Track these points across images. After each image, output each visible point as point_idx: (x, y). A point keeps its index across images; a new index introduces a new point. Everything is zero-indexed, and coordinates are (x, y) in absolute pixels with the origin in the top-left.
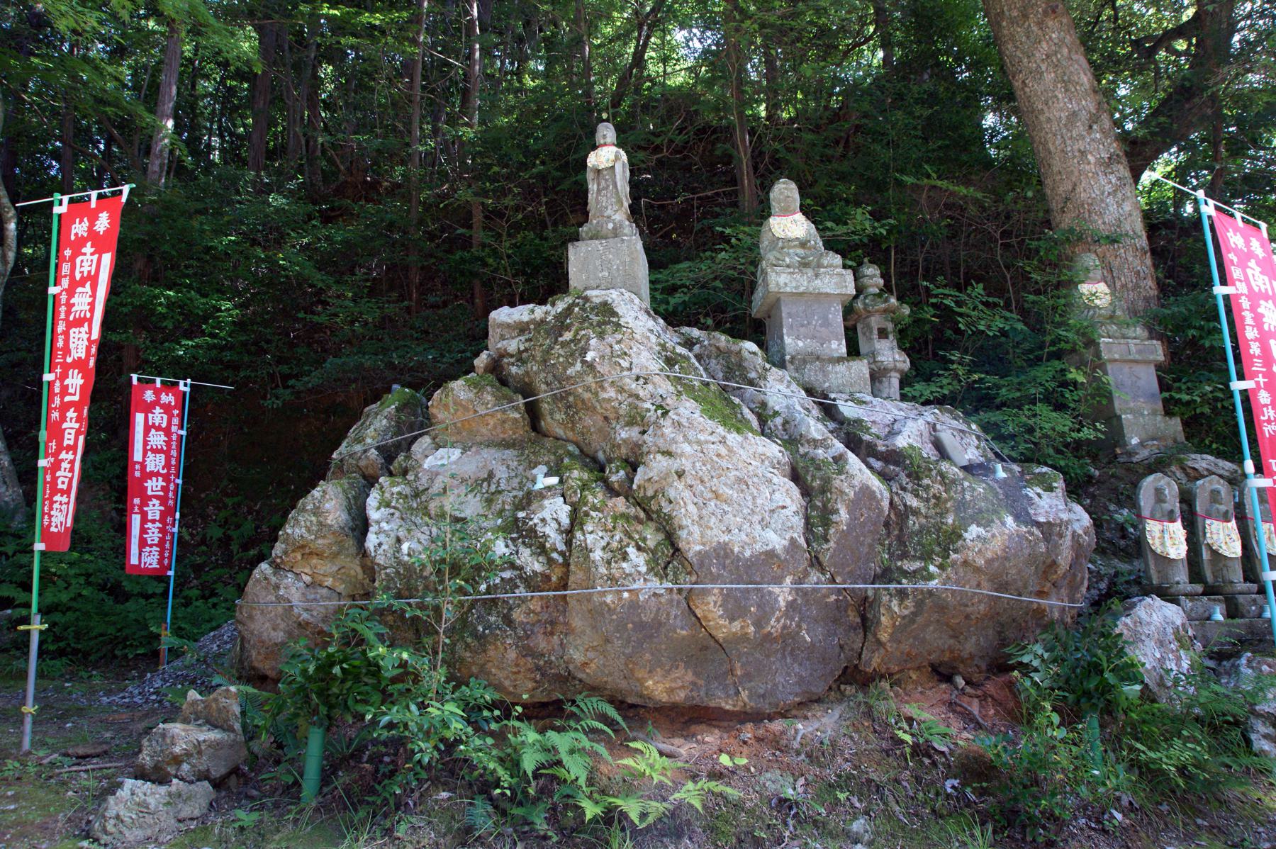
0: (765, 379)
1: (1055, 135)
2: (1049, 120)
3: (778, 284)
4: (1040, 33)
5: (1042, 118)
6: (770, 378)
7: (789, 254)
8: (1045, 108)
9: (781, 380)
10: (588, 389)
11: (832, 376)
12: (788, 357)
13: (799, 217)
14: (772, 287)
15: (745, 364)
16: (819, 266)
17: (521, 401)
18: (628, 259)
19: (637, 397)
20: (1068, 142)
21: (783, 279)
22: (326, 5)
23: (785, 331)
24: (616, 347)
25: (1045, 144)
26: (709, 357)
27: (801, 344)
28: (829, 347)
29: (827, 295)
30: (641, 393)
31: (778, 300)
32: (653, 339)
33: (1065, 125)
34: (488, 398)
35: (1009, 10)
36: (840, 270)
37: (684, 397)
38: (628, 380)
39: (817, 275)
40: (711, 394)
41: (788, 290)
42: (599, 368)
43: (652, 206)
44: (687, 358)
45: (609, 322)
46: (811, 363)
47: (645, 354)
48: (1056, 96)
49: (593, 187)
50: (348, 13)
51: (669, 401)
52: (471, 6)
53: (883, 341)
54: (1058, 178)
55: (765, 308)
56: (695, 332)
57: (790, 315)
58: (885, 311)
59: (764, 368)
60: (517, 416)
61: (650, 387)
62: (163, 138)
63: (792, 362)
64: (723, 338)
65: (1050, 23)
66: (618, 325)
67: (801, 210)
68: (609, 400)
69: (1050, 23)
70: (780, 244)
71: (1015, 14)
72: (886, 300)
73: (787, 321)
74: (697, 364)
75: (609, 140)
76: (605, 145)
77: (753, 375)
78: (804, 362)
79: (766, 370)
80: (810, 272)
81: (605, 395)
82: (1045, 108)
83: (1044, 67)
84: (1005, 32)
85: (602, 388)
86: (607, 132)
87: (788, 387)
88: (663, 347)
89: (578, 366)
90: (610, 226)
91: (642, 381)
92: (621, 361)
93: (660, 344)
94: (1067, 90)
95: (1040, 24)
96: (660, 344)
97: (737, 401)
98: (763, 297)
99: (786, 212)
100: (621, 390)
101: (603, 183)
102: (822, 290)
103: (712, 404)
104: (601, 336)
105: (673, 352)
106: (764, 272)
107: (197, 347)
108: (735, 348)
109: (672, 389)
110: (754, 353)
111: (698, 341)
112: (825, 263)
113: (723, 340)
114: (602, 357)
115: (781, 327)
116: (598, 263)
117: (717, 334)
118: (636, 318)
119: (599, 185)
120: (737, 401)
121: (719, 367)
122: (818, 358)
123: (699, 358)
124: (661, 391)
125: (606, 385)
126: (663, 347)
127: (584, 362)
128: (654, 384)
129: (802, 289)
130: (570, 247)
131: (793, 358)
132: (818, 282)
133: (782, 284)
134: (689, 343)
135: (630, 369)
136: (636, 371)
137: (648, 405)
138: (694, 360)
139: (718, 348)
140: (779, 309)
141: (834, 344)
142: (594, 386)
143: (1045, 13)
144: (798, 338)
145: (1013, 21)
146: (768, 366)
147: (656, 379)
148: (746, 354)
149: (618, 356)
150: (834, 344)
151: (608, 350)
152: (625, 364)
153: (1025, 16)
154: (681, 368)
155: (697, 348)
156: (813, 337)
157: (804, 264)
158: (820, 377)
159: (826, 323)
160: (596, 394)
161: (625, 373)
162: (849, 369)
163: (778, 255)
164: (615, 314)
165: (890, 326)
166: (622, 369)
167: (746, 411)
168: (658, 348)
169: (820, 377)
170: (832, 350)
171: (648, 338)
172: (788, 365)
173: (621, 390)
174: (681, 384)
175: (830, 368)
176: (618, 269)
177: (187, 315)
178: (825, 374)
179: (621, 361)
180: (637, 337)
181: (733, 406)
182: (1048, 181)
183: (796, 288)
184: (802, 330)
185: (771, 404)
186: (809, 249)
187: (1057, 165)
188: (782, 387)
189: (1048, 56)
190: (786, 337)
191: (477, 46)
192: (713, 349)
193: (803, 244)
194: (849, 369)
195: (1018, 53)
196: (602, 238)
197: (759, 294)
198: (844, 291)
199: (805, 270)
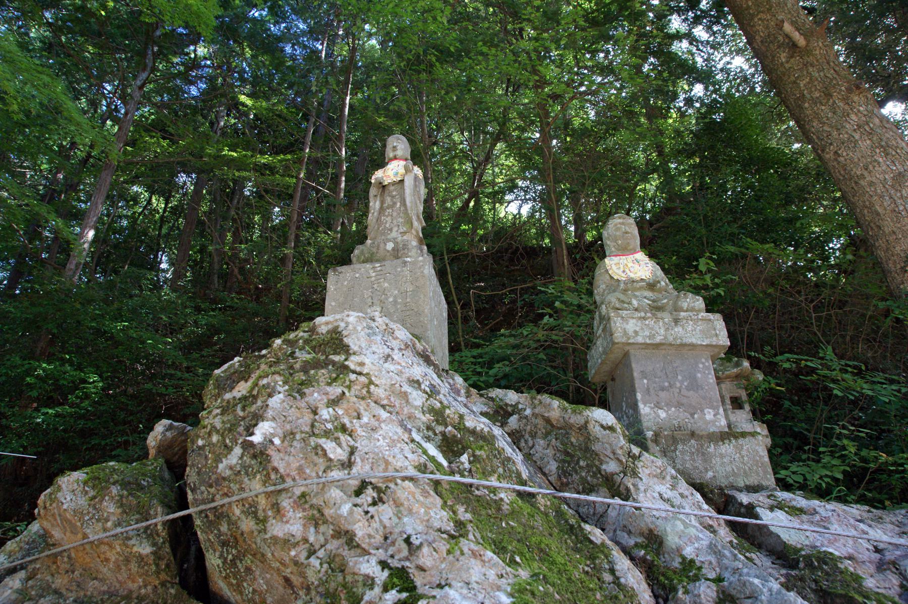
0: (635, 474)
1: (882, 197)
2: (871, 184)
3: (625, 332)
4: (846, 107)
5: (863, 183)
6: (643, 472)
7: (636, 297)
8: (866, 174)
9: (661, 477)
10: (252, 510)
11: (716, 461)
12: (649, 434)
13: (641, 256)
14: (618, 337)
15: (596, 447)
16: (677, 309)
17: (160, 518)
18: (410, 288)
19: (349, 539)
20: (899, 202)
21: (632, 326)
22: (226, 148)
23: (639, 396)
24: (325, 413)
25: (871, 207)
26: (533, 436)
27: (662, 414)
28: (702, 418)
29: (693, 346)
30: (360, 530)
31: (626, 355)
32: (417, 398)
33: (893, 186)
34: (110, 508)
35: (810, 93)
36: (704, 314)
37: (466, 545)
38: (335, 493)
39: (676, 321)
40: (538, 522)
41: (640, 339)
42: (277, 461)
43: (479, 296)
44: (488, 439)
45: (325, 364)
46: (684, 441)
47: (391, 429)
48: (876, 161)
49: (375, 205)
50: (245, 156)
51: (426, 557)
52: (341, 150)
53: (738, 412)
54: (891, 238)
55: (606, 368)
56: (511, 397)
57: (644, 375)
58: (737, 377)
59: (629, 453)
60: (146, 549)
61: (385, 512)
62: (84, 243)
63: (656, 441)
64: (556, 403)
65: (856, 98)
66: (344, 369)
67: (643, 246)
68: (287, 543)
69: (856, 98)
70: (622, 285)
71: (817, 94)
72: (737, 365)
73: (641, 384)
74: (509, 451)
75: (399, 153)
76: (395, 158)
77: (611, 467)
78: (675, 440)
79: (635, 458)
80: (667, 318)
81: (277, 529)
82: (866, 174)
83: (857, 136)
84: (809, 112)
85: (277, 508)
86: (398, 145)
87: (673, 487)
88: (439, 415)
89: (234, 457)
90: (390, 246)
91: (370, 494)
92: (329, 445)
93: (432, 410)
94: (887, 154)
95: (845, 100)
96: (432, 410)
97: (597, 535)
98: (605, 352)
99: (625, 250)
100: (317, 519)
101: (388, 200)
102: (685, 341)
103: (544, 555)
104: (298, 391)
105: (460, 425)
106: (606, 319)
107: (57, 415)
108: (576, 420)
109: (440, 517)
110: (611, 429)
111: (516, 409)
112: (685, 305)
113: (555, 407)
114: (289, 436)
115: (633, 391)
116: (367, 293)
117: (545, 398)
118: (387, 358)
119: (382, 202)
120: (597, 535)
121: (550, 452)
122: (693, 434)
123: (516, 437)
124: (411, 526)
125: (286, 503)
126: (439, 415)
127: (248, 446)
128: (398, 504)
129: (658, 339)
130: (331, 273)
131: (657, 435)
132: (678, 329)
133: (631, 333)
134: (500, 414)
135: (348, 464)
136: (361, 469)
137: (369, 567)
138: (503, 443)
139: (548, 421)
140: (629, 366)
141: (709, 415)
142: (262, 502)
143: (849, 90)
144: (658, 406)
145: (815, 101)
146: (636, 450)
147: (405, 491)
148: (596, 430)
149: (327, 434)
150: (709, 415)
151: (308, 417)
152: (336, 452)
153: (829, 95)
154: (474, 460)
155: (513, 421)
156: (679, 405)
157: (656, 308)
158: (699, 463)
159: (694, 385)
160: (262, 522)
161: (336, 474)
162: (739, 449)
163: (622, 297)
164: (345, 349)
165: (743, 395)
166: (330, 465)
167: (623, 563)
168: (427, 418)
169: (699, 463)
170: (707, 423)
171: (405, 396)
172: (650, 444)
173: (317, 519)
174: (467, 503)
175: (712, 449)
176: (395, 302)
177: (58, 388)
178: (706, 457)
179: (329, 445)
180: (379, 392)
181: (593, 552)
182: (881, 243)
183: (650, 337)
184: (663, 395)
185: (672, 540)
186: (660, 291)
187: (888, 225)
188: (664, 488)
189: (859, 126)
190: (641, 406)
191: (344, 179)
192: (540, 422)
193: (651, 286)
194: (739, 449)
195: (826, 128)
196: (378, 261)
197: (600, 346)
198: (714, 341)
199: (659, 314)
